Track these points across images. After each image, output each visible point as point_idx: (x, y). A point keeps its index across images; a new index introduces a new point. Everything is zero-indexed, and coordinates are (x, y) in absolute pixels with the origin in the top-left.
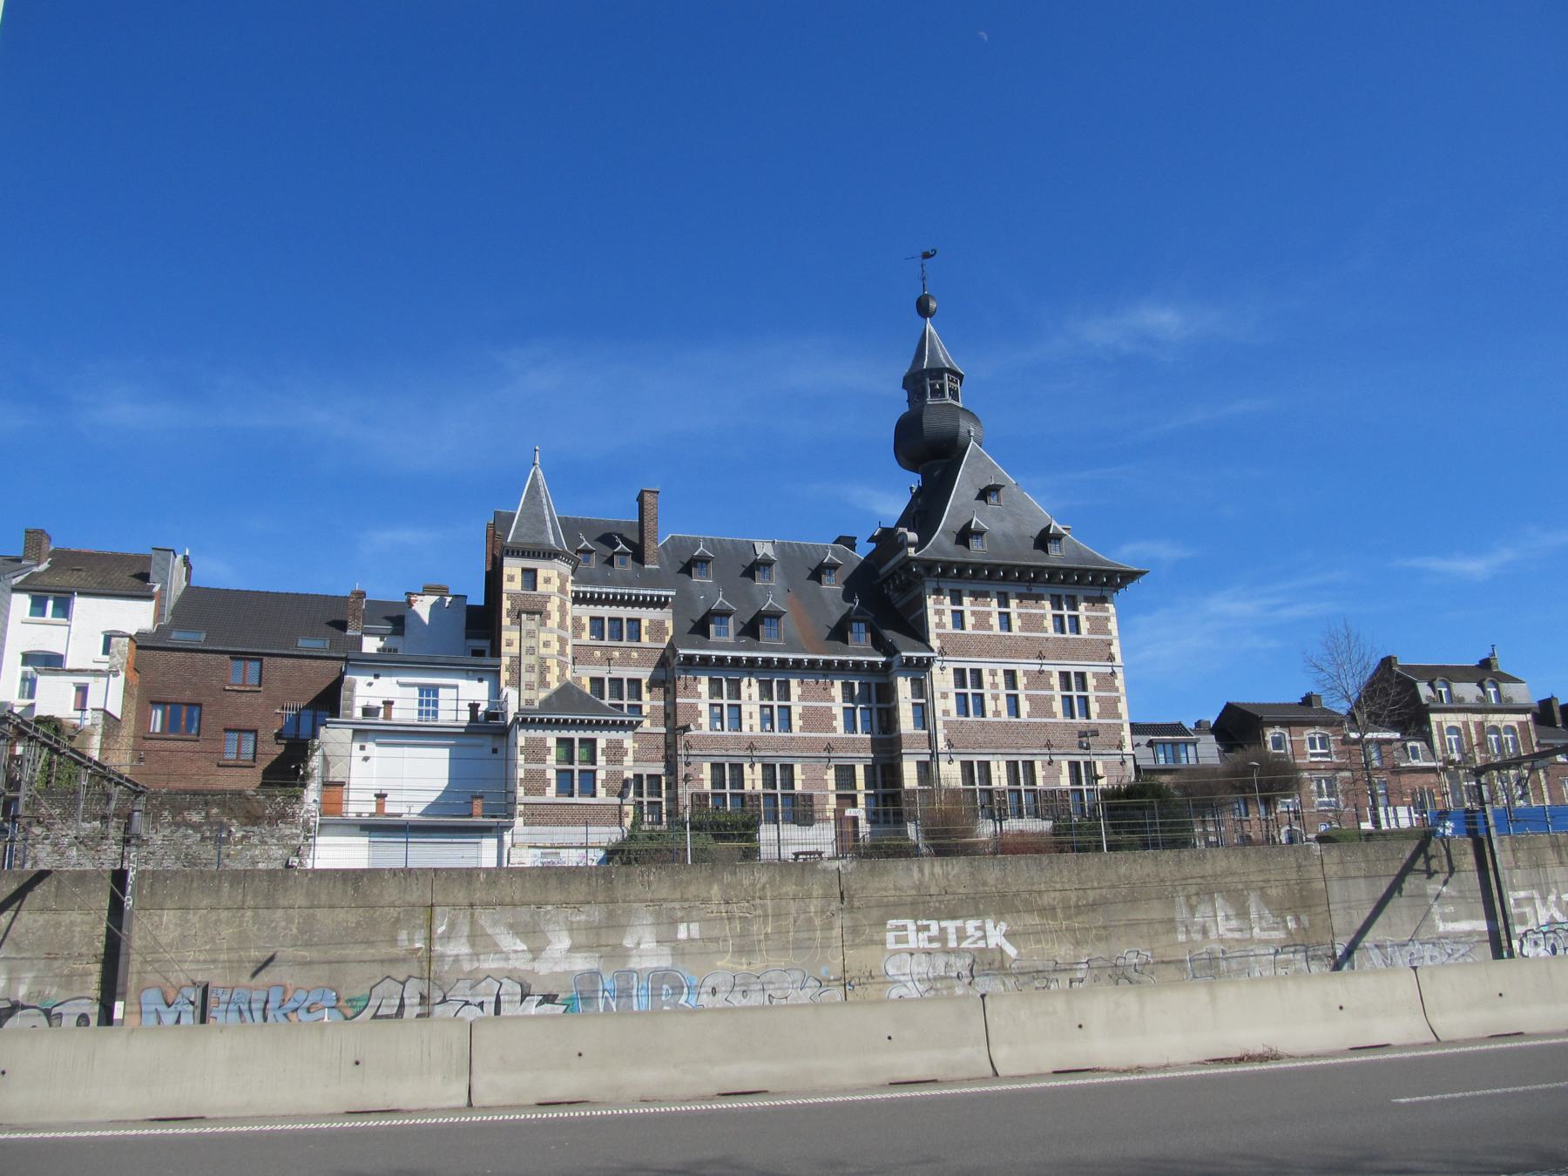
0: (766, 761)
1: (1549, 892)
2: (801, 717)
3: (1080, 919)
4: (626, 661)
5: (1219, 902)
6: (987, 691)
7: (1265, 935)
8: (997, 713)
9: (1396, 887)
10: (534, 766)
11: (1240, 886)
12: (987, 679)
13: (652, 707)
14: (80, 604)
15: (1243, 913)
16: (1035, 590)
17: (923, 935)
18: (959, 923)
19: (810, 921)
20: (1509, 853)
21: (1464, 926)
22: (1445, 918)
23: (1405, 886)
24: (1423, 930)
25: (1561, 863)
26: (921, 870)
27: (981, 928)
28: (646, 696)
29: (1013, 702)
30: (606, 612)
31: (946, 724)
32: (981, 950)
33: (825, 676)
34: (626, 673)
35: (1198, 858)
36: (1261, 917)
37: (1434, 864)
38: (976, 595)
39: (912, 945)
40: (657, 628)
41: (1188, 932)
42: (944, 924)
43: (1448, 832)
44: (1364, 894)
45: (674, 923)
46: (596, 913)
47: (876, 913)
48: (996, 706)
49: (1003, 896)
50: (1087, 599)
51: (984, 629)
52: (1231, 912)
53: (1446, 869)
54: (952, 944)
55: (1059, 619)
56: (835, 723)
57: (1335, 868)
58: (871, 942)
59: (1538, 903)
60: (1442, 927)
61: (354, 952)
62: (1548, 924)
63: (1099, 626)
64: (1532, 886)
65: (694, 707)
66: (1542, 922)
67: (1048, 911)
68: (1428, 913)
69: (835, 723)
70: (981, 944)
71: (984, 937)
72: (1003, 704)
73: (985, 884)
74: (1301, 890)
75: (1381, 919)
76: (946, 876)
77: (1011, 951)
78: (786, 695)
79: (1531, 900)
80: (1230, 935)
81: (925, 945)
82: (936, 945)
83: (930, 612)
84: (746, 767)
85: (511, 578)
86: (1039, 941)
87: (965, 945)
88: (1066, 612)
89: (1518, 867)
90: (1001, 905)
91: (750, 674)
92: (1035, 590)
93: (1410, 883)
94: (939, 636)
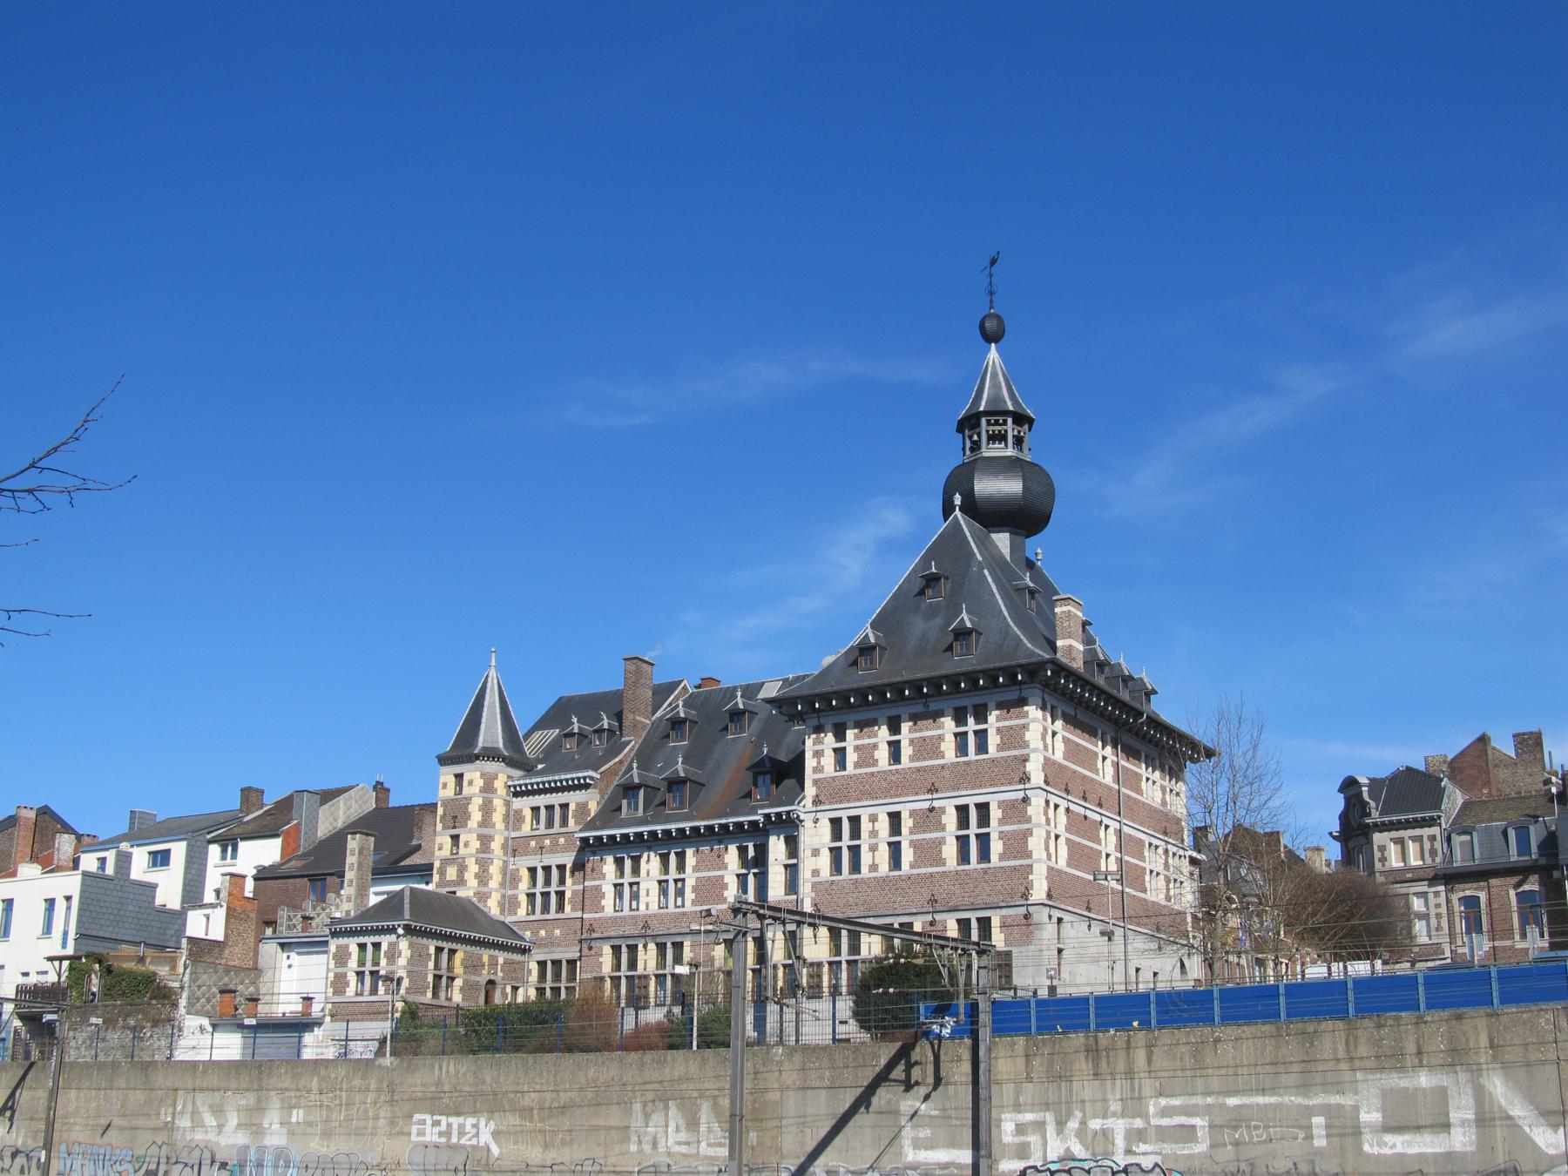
1: (1069, 1115)
2: (695, 889)
3: (552, 1122)
4: (555, 848)
5: (673, 1111)
6: (864, 842)
7: (711, 1152)
8: (874, 867)
9: (864, 1100)
10: (340, 970)
11: (695, 1094)
12: (865, 826)
13: (574, 892)
14: (242, 845)
15: (693, 1124)
16: (934, 706)
17: (436, 1130)
18: (461, 1119)
19: (366, 1111)
20: (1021, 1061)
21: (941, 1156)
22: (917, 1144)
23: (875, 1100)
24: (886, 1157)
25: (1096, 1075)
27: (476, 1126)
28: (569, 881)
29: (895, 848)
30: (541, 801)
31: (814, 886)
32: (474, 1147)
33: (720, 842)
34: (554, 860)
36: (710, 1131)
37: (916, 1073)
38: (861, 725)
39: (427, 1138)
40: (583, 808)
41: (640, 1142)
42: (451, 1120)
43: (946, 1032)
44: (823, 1108)
45: (291, 1108)
46: (249, 1099)
47: (407, 1106)
48: (875, 859)
49: (495, 1094)
50: (999, 706)
51: (868, 766)
52: (681, 1122)
53: (931, 1080)
54: (454, 1140)
55: (961, 738)
56: (726, 893)
57: (794, 1075)
58: (401, 1133)
59: (1051, 1129)
60: (911, 1155)
61: (141, 1122)
62: (1061, 1160)
63: (1013, 738)
64: (1046, 1106)
65: (598, 888)
66: (1052, 1156)
67: (526, 1112)
68: (897, 1136)
69: (726, 893)
70: (474, 1142)
71: (477, 1135)
72: (884, 852)
73: (484, 1082)
74: (754, 1101)
75: (838, 1141)
76: (457, 1072)
77: (495, 1150)
78: (681, 867)
79: (1040, 1126)
80: (677, 1149)
81: (435, 1138)
82: (443, 1140)
84: (640, 947)
85: (445, 786)
86: (516, 1142)
87: (463, 1141)
88: (972, 725)
89: (1029, 1079)
90: (490, 1103)
91: (649, 849)
92: (934, 706)
93: (881, 1098)
94: (815, 782)
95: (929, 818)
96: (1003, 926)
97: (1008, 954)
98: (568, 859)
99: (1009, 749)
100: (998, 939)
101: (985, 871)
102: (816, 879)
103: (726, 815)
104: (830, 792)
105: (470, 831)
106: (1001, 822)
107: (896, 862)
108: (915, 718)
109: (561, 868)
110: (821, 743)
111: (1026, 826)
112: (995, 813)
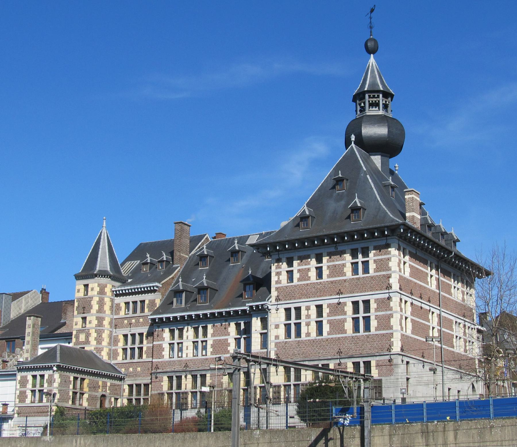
0: (193, 373)
2: (212, 346)
4: (137, 324)
6: (303, 321)
8: (308, 334)
12: (304, 312)
13: (148, 347)
16: (340, 248)
20: (387, 438)
26: (76, 442)
28: (145, 342)
29: (319, 324)
30: (130, 299)
31: (276, 344)
33: (226, 321)
34: (137, 331)
35: (193, 439)
43: (347, 422)
48: (309, 330)
50: (375, 248)
51: (305, 280)
55: (355, 265)
56: (229, 348)
63: (383, 265)
65: (160, 346)
72: (313, 326)
78: (205, 334)
83: (273, 274)
84: (183, 377)
88: (360, 258)
91: (188, 324)
92: (340, 248)
94: (277, 289)
95: (338, 308)
96: (377, 366)
97: (380, 381)
98: (145, 330)
99: (380, 271)
100: (375, 373)
101: (368, 337)
102: (277, 341)
103: (229, 306)
104: (285, 294)
105: (92, 315)
106: (376, 310)
107: (320, 331)
108: (330, 255)
109: (141, 335)
110: (280, 268)
111: (389, 312)
112: (373, 306)
